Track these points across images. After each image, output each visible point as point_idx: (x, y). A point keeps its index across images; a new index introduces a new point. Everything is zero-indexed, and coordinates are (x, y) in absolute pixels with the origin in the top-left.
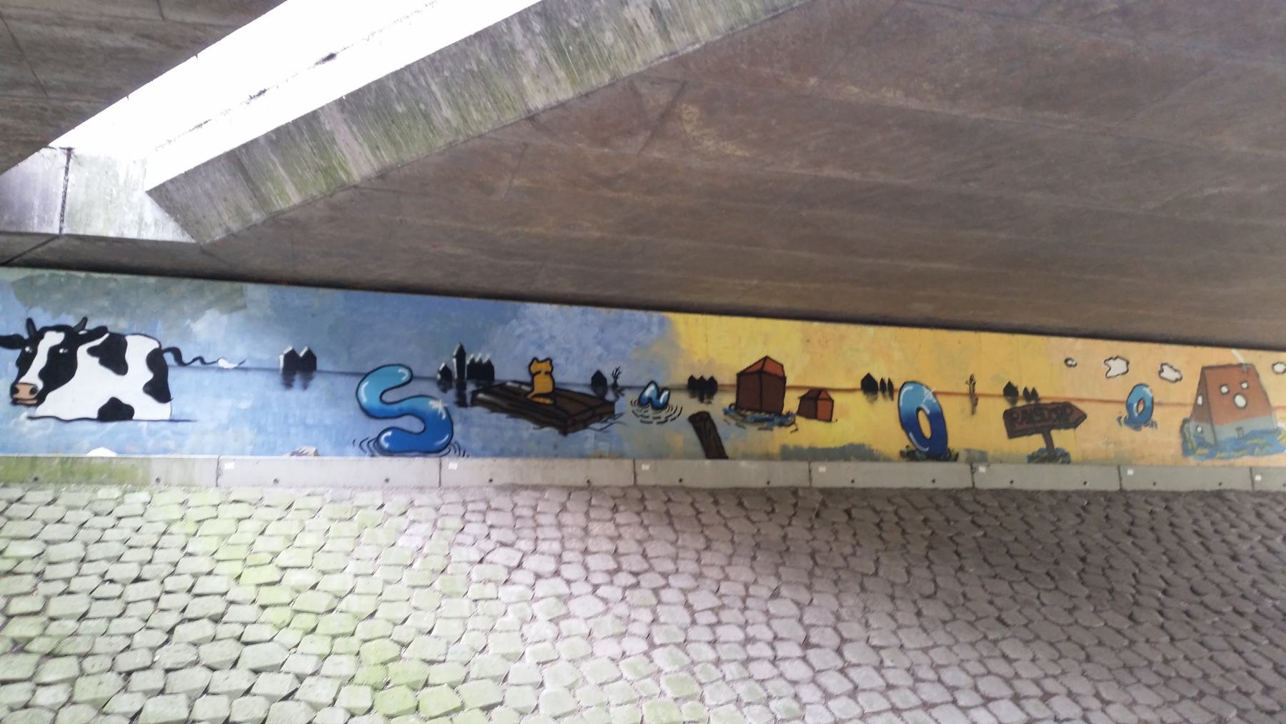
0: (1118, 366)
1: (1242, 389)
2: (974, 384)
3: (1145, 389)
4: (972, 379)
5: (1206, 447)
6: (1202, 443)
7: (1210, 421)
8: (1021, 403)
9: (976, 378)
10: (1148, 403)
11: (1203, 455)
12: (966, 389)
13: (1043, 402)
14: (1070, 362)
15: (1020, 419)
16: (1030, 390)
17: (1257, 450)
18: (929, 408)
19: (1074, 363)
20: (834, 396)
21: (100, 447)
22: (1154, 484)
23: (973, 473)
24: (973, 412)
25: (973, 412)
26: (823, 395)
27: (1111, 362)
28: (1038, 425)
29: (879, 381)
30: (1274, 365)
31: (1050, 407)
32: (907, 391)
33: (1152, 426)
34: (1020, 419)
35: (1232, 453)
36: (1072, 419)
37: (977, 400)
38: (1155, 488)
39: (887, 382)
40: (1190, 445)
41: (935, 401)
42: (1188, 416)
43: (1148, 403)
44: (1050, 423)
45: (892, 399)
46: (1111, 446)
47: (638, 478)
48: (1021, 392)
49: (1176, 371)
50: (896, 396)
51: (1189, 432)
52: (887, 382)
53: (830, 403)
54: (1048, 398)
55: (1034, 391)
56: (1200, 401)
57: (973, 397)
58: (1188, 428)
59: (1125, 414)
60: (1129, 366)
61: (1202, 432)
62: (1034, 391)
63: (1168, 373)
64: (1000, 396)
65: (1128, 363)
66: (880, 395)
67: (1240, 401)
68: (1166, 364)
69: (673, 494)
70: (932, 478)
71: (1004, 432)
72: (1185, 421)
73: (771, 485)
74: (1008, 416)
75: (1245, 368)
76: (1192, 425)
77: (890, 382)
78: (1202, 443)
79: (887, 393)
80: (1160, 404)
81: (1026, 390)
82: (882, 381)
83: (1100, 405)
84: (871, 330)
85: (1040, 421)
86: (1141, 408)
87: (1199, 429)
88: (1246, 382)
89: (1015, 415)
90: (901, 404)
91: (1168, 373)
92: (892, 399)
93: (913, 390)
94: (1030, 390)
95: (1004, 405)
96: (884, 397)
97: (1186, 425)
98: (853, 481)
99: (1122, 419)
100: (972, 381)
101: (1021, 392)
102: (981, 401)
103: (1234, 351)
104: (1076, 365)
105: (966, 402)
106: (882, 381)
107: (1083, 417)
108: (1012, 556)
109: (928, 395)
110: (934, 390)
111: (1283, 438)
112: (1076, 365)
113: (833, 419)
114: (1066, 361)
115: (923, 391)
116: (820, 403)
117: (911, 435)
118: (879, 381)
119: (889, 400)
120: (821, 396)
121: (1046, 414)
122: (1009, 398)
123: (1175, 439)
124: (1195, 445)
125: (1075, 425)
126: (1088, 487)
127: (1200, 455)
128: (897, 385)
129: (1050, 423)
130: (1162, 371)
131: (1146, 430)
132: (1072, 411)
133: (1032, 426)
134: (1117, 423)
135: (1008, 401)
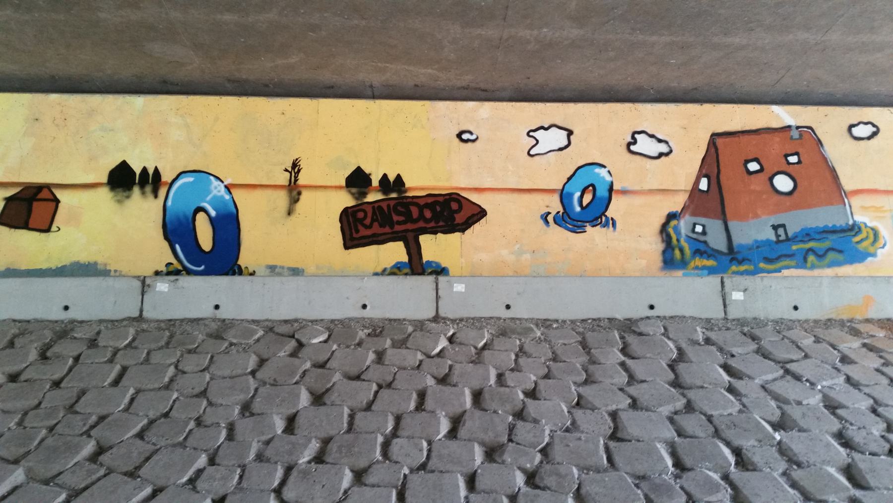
0: (553, 139)
1: (789, 163)
2: (299, 171)
3: (598, 170)
4: (295, 165)
5: (709, 257)
6: (702, 250)
7: (724, 217)
8: (373, 197)
9: (302, 164)
10: (602, 192)
11: (704, 268)
12: (283, 179)
13: (410, 194)
14: (465, 136)
15: (368, 221)
16: (392, 178)
17: (811, 258)
18: (214, 209)
19: (473, 137)
20: (59, 194)
21: (825, 159)
22: (508, 307)
23: (143, 293)
24: (289, 213)
25: (289, 213)
26: (44, 194)
27: (539, 135)
28: (398, 228)
29: (138, 171)
30: (852, 126)
31: (422, 202)
32: (184, 184)
33: (606, 225)
34: (368, 221)
35: (762, 265)
36: (459, 218)
37: (299, 193)
38: (795, 315)
39: (151, 171)
40: (677, 253)
41: (227, 197)
42: (677, 208)
43: (602, 192)
44: (421, 224)
45: (156, 197)
46: (527, 256)
47: (729, 309)
48: (375, 183)
49: (660, 141)
50: (162, 192)
51: (678, 233)
52: (151, 171)
53: (54, 204)
54: (422, 189)
55: (399, 178)
56: (704, 185)
57: (294, 191)
58: (676, 229)
59: (556, 206)
60: (572, 137)
61: (704, 233)
62: (399, 178)
63: (644, 145)
64: (339, 187)
65: (570, 133)
66: (136, 190)
67: (783, 183)
68: (640, 133)
69: (629, 336)
70: (656, 306)
71: (338, 238)
72: (671, 216)
73: (222, 314)
74: (349, 219)
75: (795, 134)
76: (684, 225)
77: (156, 171)
78: (702, 250)
79: (148, 189)
80: (624, 192)
81: (385, 176)
82: (145, 170)
83: (516, 196)
84: (139, 101)
85: (404, 222)
86: (587, 198)
87: (699, 229)
88: (797, 154)
89: (361, 215)
90: (169, 203)
91: (644, 145)
92: (156, 197)
93: (192, 182)
94: (392, 178)
95: (347, 200)
96: (143, 193)
97: (673, 223)
98: (217, 307)
99: (550, 218)
100: (295, 167)
101: (375, 183)
102: (306, 195)
103: (776, 108)
104: (477, 138)
105: (282, 198)
106: (145, 170)
107: (480, 213)
108: (847, 443)
109: (218, 189)
110: (226, 183)
111: (862, 240)
112: (477, 138)
113: (54, 228)
114: (459, 136)
115: (210, 183)
116: (35, 204)
117: (178, 247)
118: (138, 171)
119: (151, 197)
120: (40, 196)
121: (415, 211)
122: (354, 190)
123: (654, 246)
124: (688, 251)
125: (464, 227)
126: (367, 313)
127: (697, 268)
128: (167, 177)
129: (421, 224)
130: (635, 142)
131: (593, 233)
132: (461, 208)
133: (387, 229)
134: (542, 222)
135: (353, 194)
